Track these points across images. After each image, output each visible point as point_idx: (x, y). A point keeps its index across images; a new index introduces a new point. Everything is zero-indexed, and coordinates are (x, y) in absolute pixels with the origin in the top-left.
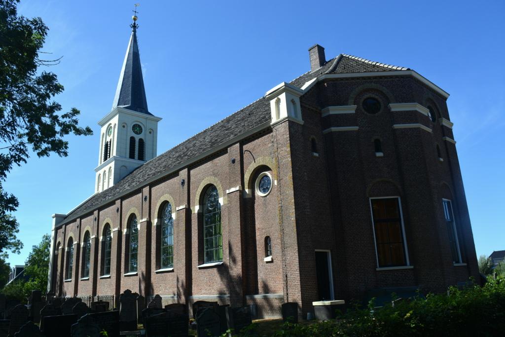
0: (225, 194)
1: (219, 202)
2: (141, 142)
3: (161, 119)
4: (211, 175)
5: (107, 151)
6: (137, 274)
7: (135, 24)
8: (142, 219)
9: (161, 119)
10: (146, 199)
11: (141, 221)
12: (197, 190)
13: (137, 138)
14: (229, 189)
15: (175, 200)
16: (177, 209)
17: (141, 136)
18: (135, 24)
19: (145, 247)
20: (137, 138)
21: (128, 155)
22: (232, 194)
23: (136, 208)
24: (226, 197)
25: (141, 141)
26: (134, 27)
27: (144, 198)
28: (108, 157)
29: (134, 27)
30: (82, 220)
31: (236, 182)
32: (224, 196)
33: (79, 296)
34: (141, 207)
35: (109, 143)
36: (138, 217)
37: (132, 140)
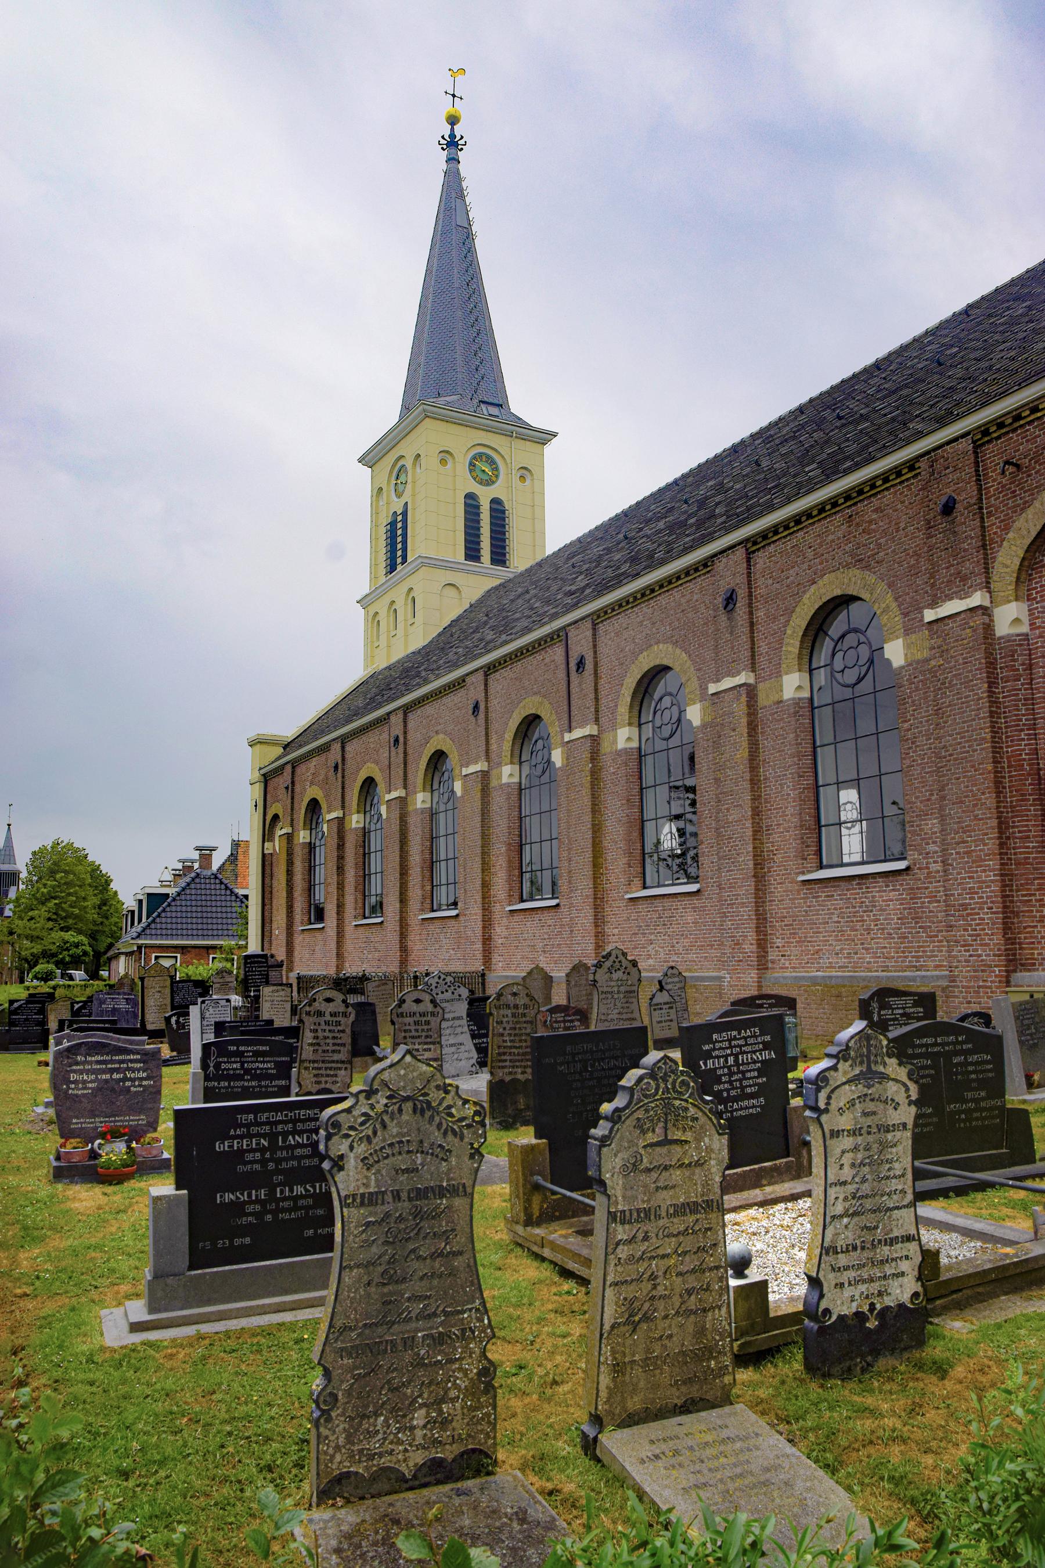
0: (703, 695)
1: (553, 759)
2: (498, 510)
3: (554, 435)
4: (848, 566)
5: (396, 536)
6: (558, 905)
7: (452, 135)
8: (570, 730)
9: (554, 435)
10: (581, 664)
11: (388, 797)
12: (786, 624)
13: (485, 496)
14: (933, 604)
15: (694, 662)
16: (566, 739)
17: (496, 490)
18: (452, 135)
19: (284, 894)
20: (485, 496)
21: (460, 555)
22: (727, 697)
23: (544, 696)
24: (707, 703)
25: (496, 502)
26: (452, 144)
27: (392, 740)
28: (399, 560)
29: (452, 144)
30: (348, 748)
31: (964, 579)
32: (907, 632)
33: (417, 967)
34: (565, 693)
35: (400, 518)
36: (381, 787)
37: (471, 503)
